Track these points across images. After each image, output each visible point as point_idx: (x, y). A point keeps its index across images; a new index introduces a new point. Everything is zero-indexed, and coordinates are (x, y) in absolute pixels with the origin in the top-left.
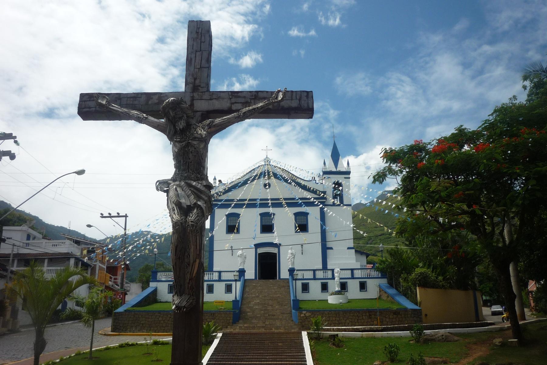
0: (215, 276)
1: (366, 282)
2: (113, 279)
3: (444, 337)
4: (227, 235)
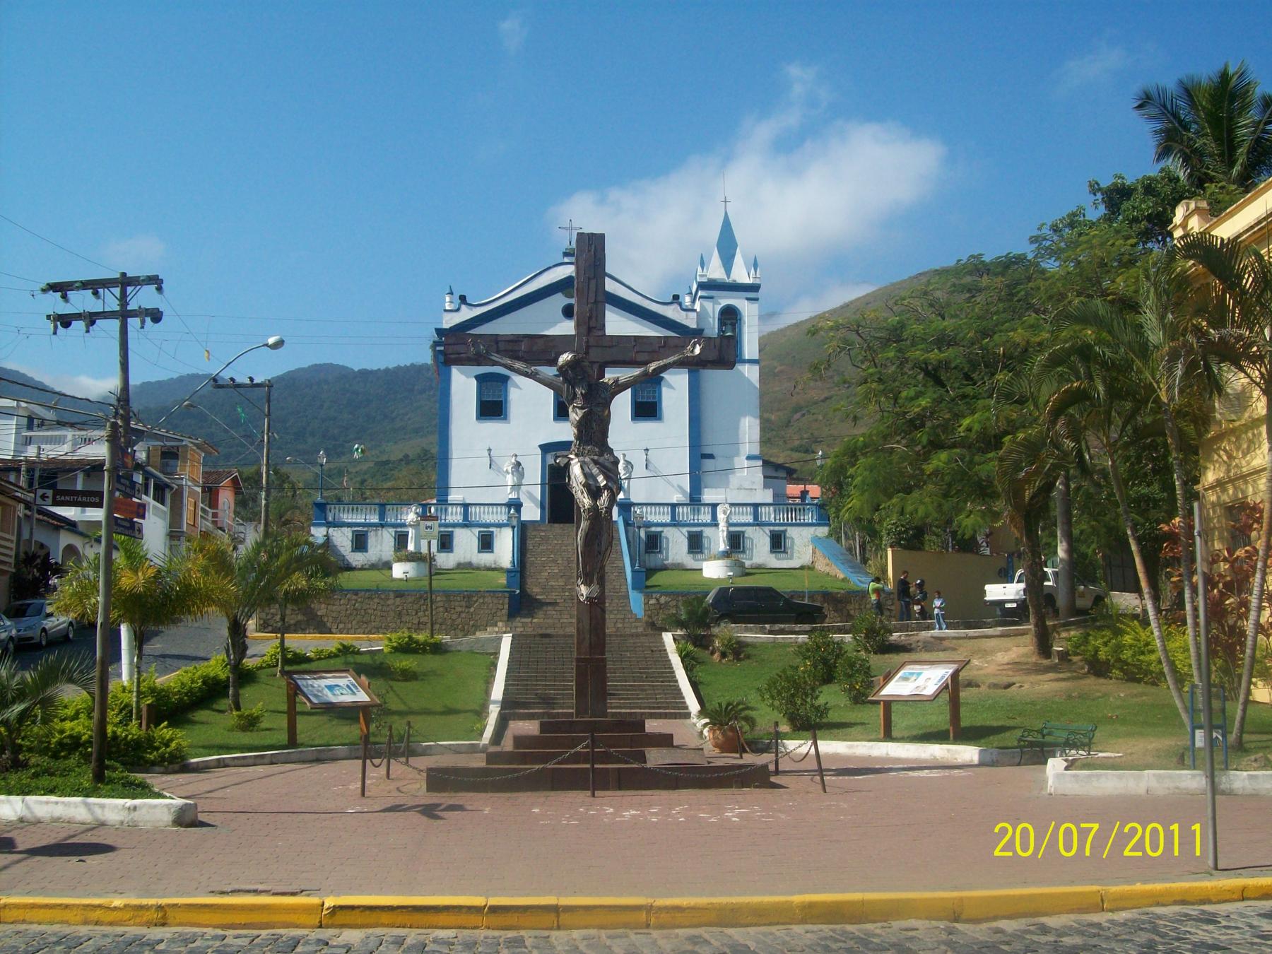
0: (455, 515)
1: (743, 532)
2: (210, 515)
3: (919, 644)
4: (495, 549)
